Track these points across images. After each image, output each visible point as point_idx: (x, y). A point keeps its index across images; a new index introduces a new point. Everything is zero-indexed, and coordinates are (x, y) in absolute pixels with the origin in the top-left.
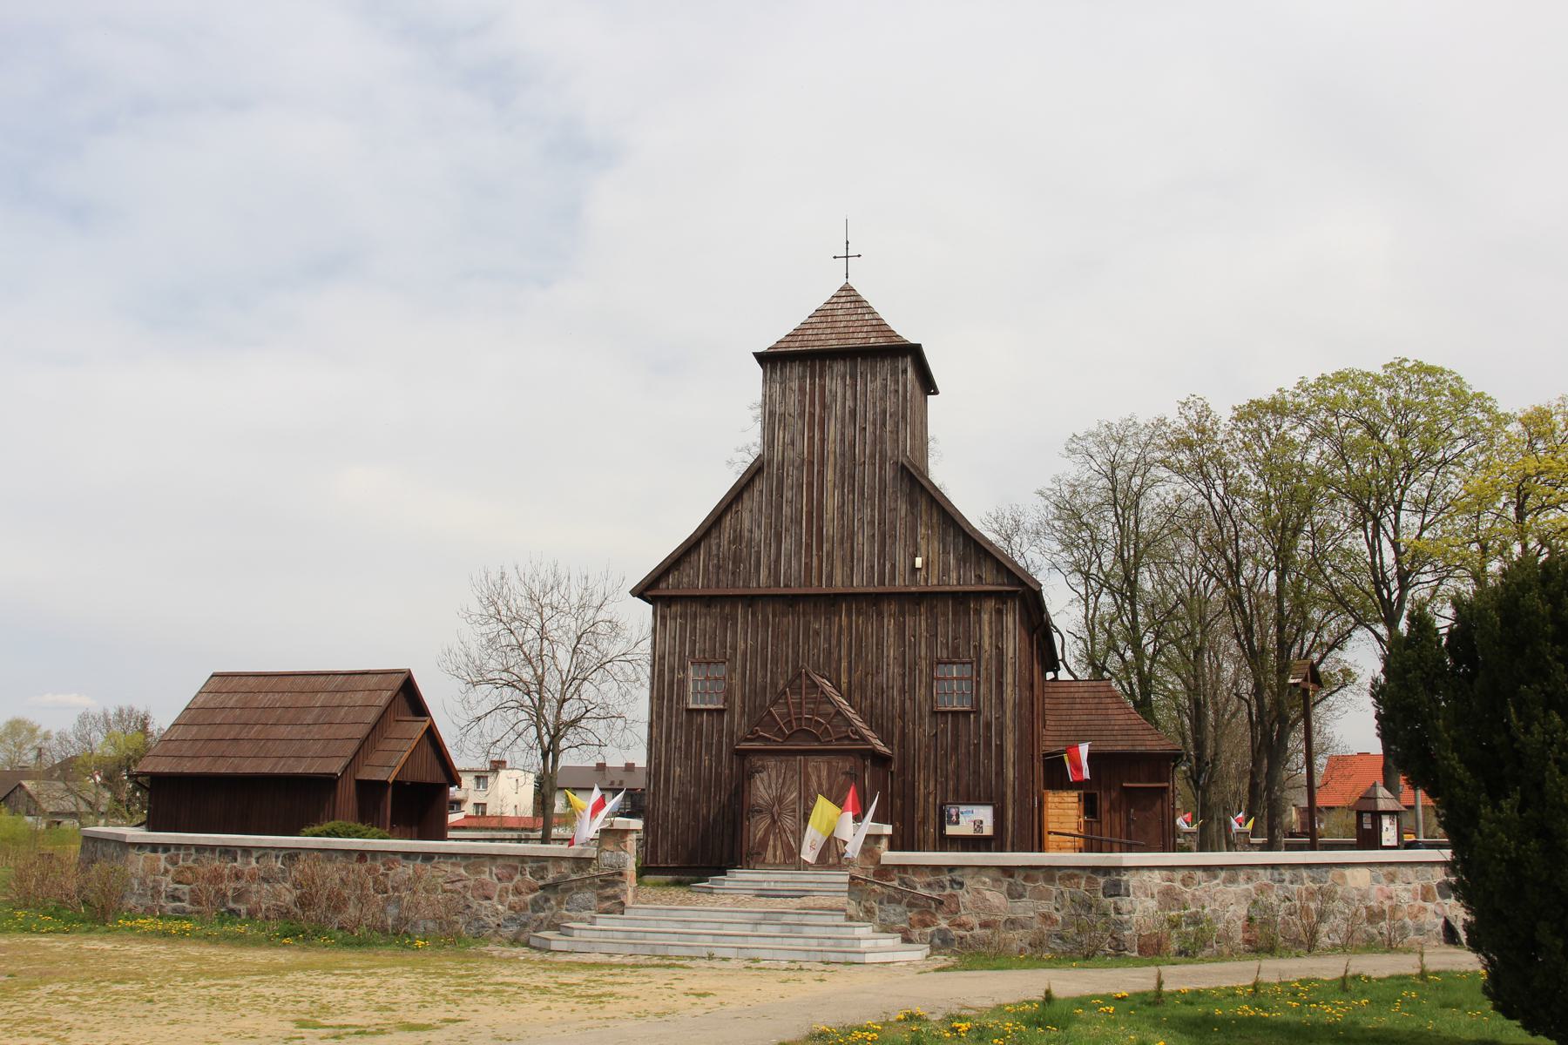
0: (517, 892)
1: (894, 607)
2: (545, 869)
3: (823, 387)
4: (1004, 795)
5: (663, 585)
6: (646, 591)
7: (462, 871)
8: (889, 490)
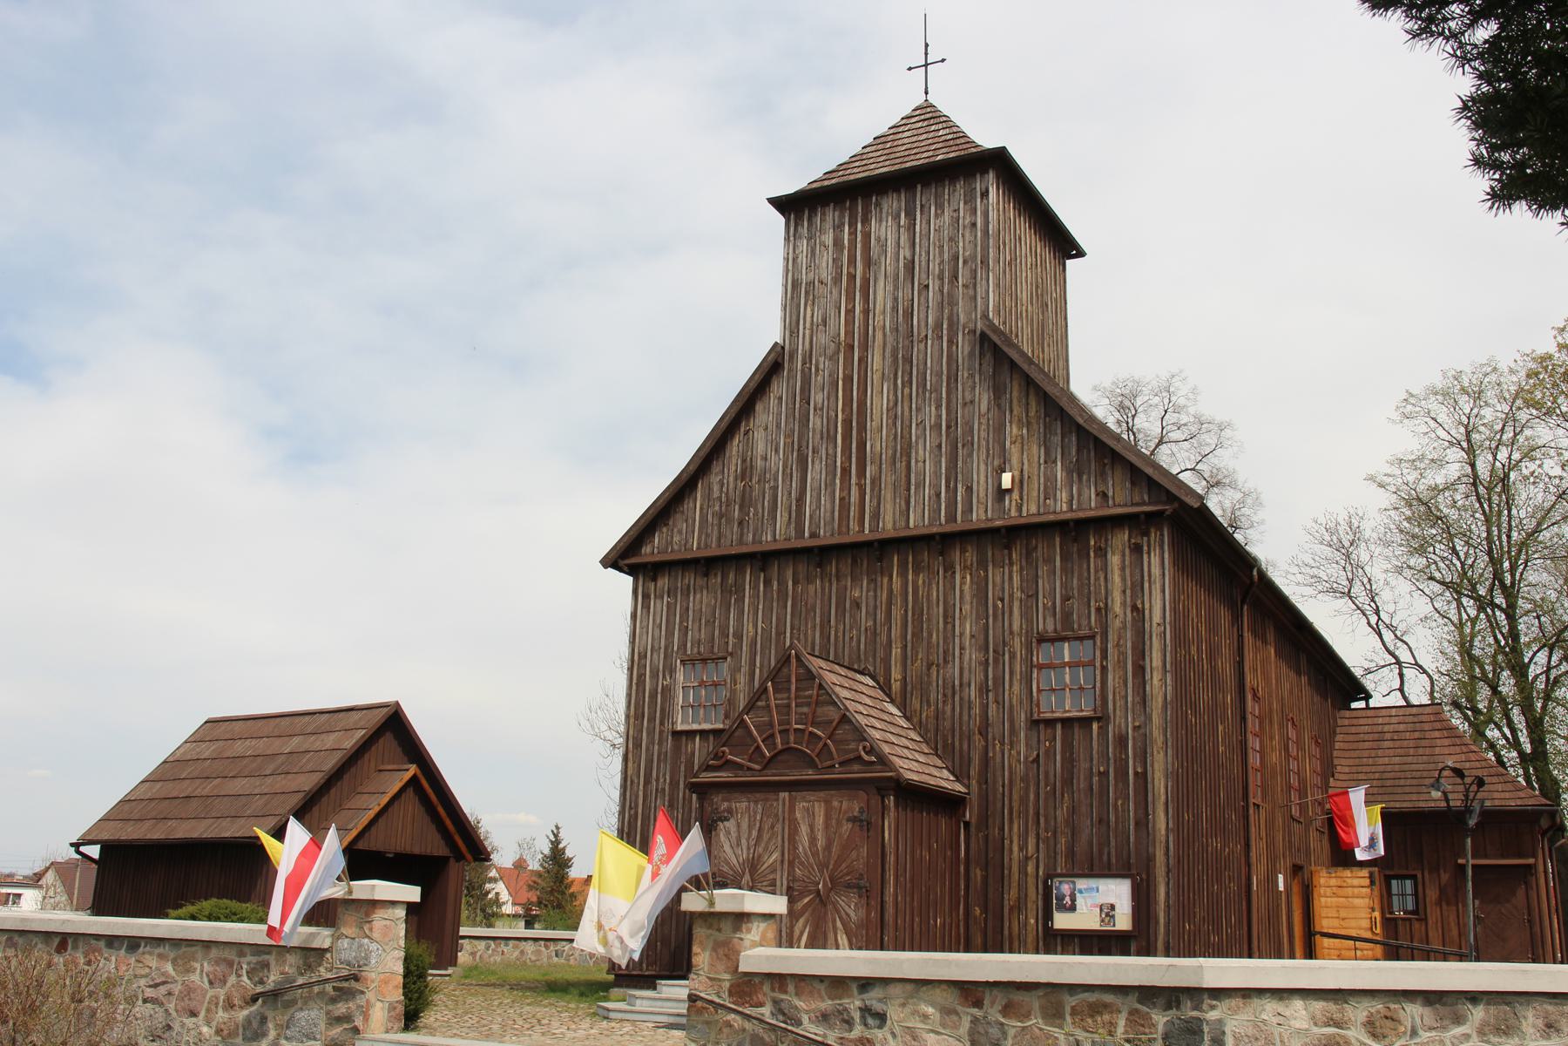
0: (229, 1005)
1: (971, 556)
2: (266, 965)
3: (867, 236)
4: (1150, 859)
5: (647, 549)
6: (623, 557)
7: (169, 968)
8: (963, 374)
